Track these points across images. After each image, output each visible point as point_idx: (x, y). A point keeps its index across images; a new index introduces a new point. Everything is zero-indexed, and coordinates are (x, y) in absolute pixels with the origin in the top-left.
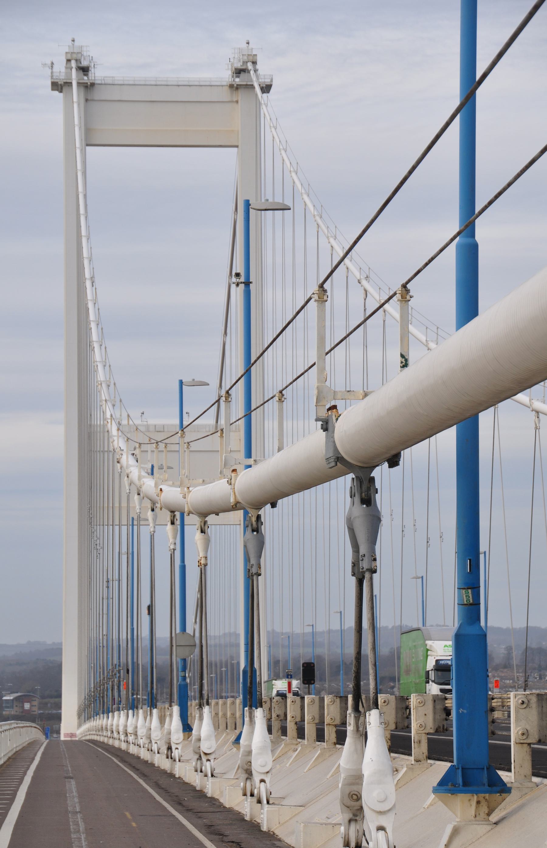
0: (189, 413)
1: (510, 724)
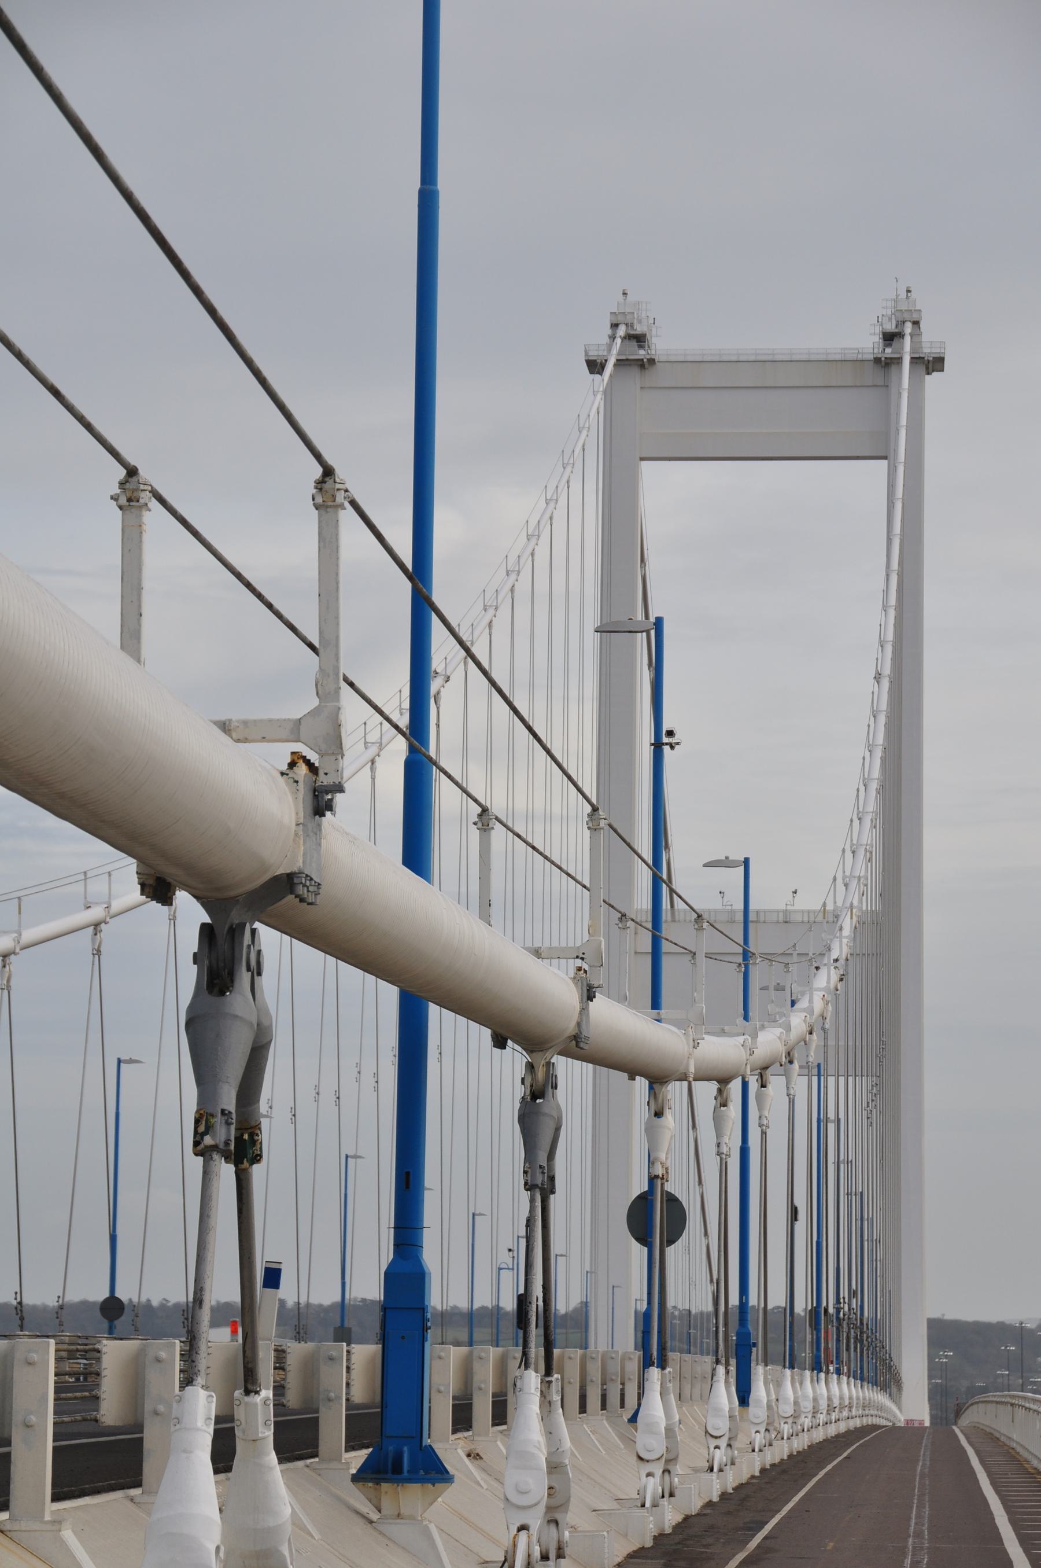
0: (723, 893)
1: (506, 1396)
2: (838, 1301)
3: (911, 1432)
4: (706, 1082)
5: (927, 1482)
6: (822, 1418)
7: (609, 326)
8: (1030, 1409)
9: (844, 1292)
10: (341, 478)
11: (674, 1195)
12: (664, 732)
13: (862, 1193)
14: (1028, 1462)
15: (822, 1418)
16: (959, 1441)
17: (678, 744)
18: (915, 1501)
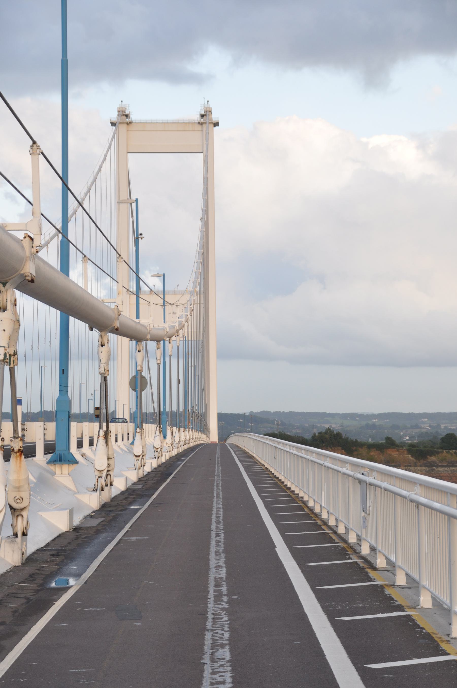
2: (192, 407)
3: (213, 445)
4: (153, 342)
5: (219, 460)
6: (187, 442)
7: (117, 111)
8: (249, 437)
9: (193, 405)
10: (39, 145)
11: (144, 376)
12: (139, 234)
13: (198, 375)
14: (249, 453)
15: (190, 441)
16: (228, 447)
17: (143, 238)
18: (216, 465)
